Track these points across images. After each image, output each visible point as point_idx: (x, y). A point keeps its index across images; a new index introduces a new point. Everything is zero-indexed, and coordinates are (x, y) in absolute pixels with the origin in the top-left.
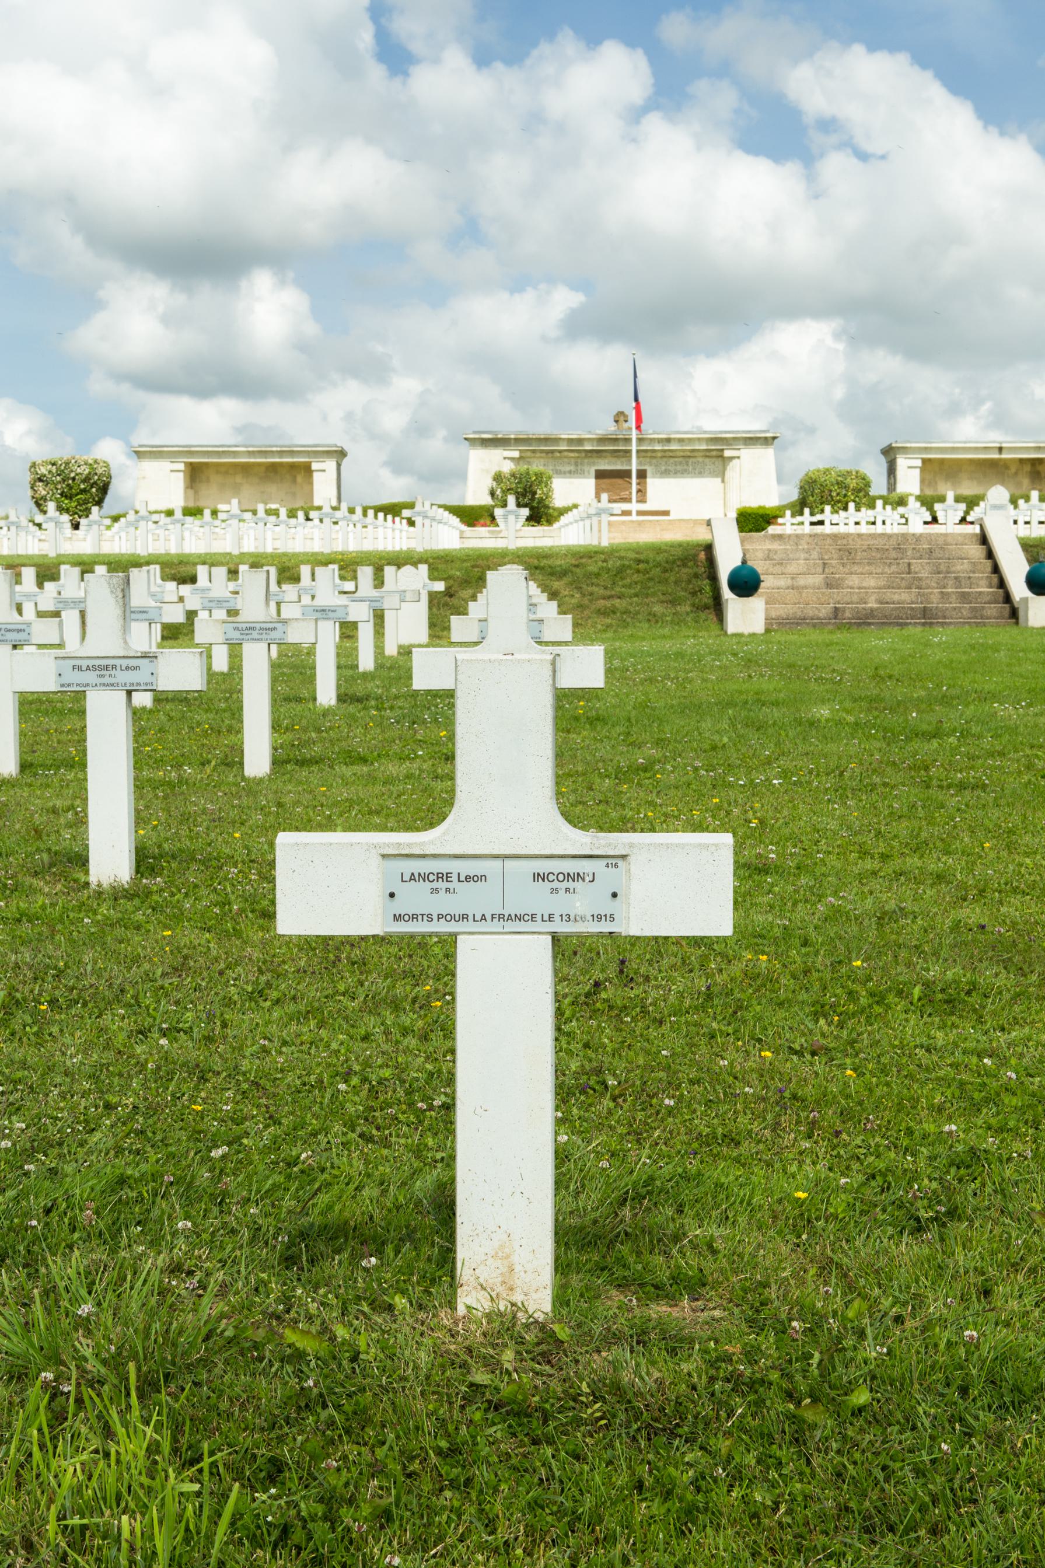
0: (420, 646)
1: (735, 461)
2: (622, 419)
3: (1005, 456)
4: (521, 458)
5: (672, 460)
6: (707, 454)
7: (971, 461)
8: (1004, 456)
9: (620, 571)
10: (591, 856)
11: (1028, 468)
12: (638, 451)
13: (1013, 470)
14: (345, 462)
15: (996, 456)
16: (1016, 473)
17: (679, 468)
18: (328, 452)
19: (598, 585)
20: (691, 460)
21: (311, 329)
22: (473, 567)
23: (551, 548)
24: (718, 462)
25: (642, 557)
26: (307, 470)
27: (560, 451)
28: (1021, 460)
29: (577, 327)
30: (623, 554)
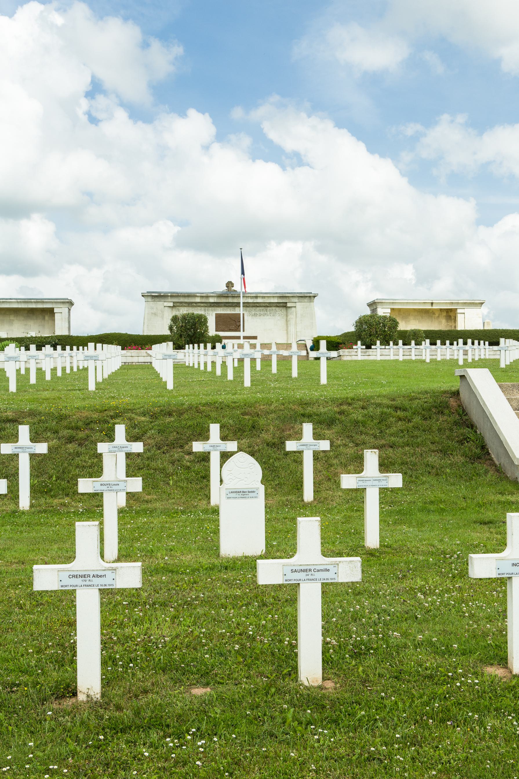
0: (261, 557)
1: (293, 309)
2: (230, 285)
3: (434, 307)
4: (174, 306)
5: (258, 308)
6: (278, 305)
7: (415, 310)
8: (434, 307)
9: (383, 419)
10: (102, 540)
11: (444, 314)
12: (244, 303)
13: (437, 315)
14: (73, 309)
15: (429, 307)
16: (438, 317)
17: (262, 313)
18: (63, 303)
19: (367, 434)
20: (268, 308)
21: (461, 119)
22: (243, 414)
23: (11, 322)
24: (284, 310)
25: (397, 403)
26: (51, 312)
27: (196, 303)
28: (441, 310)
29: (182, 243)
30: (378, 401)
